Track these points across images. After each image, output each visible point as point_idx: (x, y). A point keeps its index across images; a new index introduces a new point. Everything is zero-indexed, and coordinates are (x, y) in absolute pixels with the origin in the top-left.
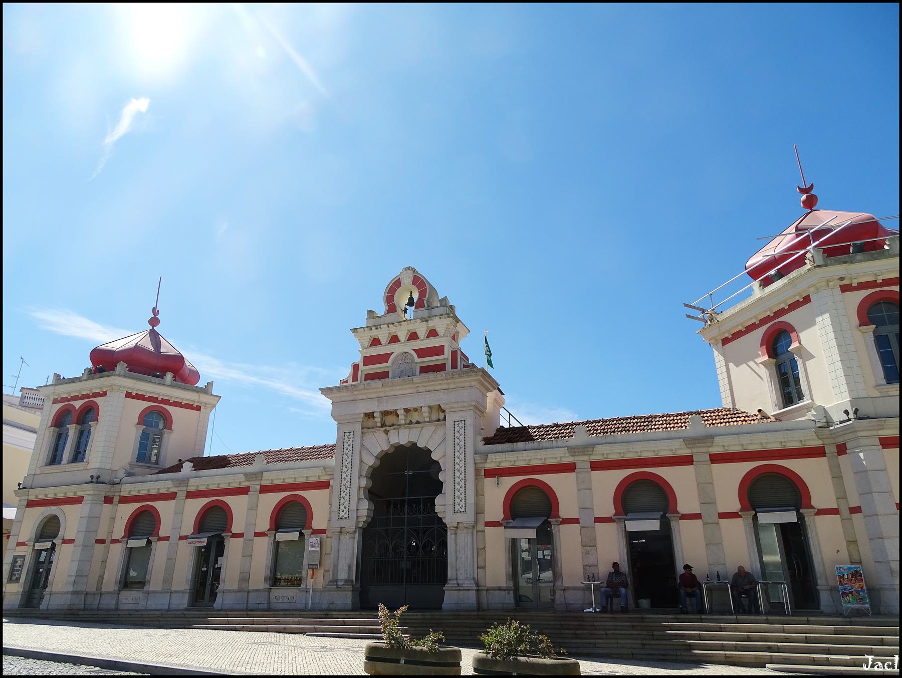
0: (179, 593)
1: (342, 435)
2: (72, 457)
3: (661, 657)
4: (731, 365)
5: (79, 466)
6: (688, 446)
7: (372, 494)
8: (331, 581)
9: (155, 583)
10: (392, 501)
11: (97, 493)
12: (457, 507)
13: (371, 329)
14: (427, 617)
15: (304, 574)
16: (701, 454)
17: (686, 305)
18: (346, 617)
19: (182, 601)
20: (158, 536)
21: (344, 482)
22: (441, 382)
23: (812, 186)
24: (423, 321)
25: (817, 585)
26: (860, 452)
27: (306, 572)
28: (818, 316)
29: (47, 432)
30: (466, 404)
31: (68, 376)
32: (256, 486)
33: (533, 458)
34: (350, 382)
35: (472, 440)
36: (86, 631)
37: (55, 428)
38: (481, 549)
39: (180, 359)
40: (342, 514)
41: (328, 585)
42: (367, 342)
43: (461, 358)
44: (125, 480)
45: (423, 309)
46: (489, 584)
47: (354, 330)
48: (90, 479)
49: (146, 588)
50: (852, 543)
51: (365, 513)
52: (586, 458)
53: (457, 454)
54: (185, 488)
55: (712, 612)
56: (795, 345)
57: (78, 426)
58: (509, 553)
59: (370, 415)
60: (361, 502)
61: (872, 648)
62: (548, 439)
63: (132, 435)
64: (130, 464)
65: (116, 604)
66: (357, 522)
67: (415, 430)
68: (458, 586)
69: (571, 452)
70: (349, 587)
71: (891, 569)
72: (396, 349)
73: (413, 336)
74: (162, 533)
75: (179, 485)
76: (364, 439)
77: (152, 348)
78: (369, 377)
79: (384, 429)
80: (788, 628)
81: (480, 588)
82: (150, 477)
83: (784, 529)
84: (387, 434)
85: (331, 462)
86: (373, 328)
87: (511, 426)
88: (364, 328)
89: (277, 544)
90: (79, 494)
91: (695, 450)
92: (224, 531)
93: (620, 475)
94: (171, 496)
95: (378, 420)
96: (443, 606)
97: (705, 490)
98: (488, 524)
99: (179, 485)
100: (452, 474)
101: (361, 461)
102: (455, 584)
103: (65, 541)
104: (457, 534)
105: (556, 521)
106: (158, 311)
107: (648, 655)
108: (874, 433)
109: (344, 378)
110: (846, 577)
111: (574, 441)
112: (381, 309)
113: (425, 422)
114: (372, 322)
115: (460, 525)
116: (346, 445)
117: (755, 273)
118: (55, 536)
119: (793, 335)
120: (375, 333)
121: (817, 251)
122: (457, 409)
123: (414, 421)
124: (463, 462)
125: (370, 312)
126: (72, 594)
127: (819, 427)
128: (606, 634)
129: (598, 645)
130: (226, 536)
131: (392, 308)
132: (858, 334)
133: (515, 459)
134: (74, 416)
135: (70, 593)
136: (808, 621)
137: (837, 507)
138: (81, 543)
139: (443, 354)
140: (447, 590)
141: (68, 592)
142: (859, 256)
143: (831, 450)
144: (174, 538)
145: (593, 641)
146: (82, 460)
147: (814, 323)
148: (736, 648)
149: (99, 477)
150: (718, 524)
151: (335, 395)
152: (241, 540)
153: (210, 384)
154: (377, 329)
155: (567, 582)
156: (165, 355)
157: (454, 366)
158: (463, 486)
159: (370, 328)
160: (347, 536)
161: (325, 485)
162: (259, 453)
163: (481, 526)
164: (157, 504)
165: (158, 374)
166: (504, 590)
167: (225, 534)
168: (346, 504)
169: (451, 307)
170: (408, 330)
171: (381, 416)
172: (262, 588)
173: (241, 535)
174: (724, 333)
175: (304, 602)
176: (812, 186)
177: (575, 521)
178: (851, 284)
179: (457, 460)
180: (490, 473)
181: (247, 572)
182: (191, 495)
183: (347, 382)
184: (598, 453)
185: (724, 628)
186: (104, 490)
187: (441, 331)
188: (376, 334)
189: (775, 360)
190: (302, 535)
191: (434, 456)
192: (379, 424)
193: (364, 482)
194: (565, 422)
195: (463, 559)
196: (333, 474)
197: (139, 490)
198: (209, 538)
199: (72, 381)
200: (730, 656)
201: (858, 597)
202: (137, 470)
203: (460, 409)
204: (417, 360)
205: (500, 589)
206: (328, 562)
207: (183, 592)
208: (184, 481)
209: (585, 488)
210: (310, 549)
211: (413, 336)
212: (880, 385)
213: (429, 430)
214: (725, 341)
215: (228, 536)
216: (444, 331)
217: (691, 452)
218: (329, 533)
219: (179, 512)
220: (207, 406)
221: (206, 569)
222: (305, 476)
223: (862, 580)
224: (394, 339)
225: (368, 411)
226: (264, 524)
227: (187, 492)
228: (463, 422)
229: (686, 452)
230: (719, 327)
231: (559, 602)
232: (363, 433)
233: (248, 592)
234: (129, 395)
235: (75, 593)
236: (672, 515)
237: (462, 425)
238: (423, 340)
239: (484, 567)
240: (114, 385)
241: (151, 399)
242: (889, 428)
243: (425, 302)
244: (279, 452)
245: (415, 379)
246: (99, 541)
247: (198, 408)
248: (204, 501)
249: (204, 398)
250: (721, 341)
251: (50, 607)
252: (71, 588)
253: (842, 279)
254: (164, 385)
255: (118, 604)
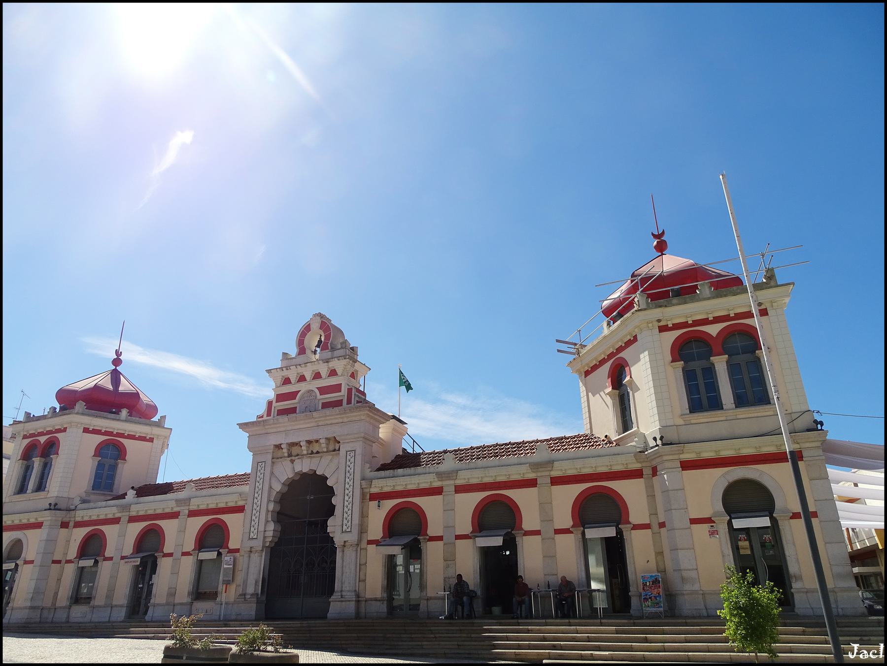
0: (185, 605)
1: (256, 464)
2: (18, 489)
3: (467, 656)
4: (590, 394)
5: (41, 494)
6: (533, 470)
7: (280, 517)
8: (240, 595)
9: (99, 599)
10: (319, 521)
11: (54, 518)
12: (345, 527)
13: (283, 370)
14: (304, 625)
15: (220, 589)
16: (543, 478)
17: (558, 341)
18: (240, 626)
19: (120, 614)
20: (104, 556)
21: (255, 506)
22: (336, 417)
23: (663, 232)
24: (325, 363)
25: (630, 591)
26: (665, 474)
27: (221, 587)
28: (641, 353)
29: (17, 464)
30: (356, 436)
31: (38, 414)
32: (185, 511)
33: (408, 483)
34: (265, 418)
35: (358, 467)
36: (110, 642)
37: (41, 458)
38: (363, 565)
39: (136, 396)
40: (252, 535)
41: (237, 598)
42: (279, 381)
43: (355, 394)
44: (80, 506)
45: (327, 351)
46: (369, 595)
47: (269, 371)
48: (48, 507)
49: (92, 603)
50: (660, 554)
51: (271, 534)
52: (452, 482)
53: (347, 480)
54: (128, 514)
55: (537, 618)
56: (628, 378)
57: (24, 461)
58: (385, 567)
59: (278, 447)
60: (268, 524)
61: (632, 645)
62: (564, 450)
63: (87, 466)
64: (85, 492)
65: (66, 618)
66: (264, 542)
67: (315, 459)
68: (342, 598)
69: (439, 477)
70: (254, 599)
71: (682, 577)
72: (303, 387)
73: (317, 376)
74: (107, 554)
75: (122, 511)
76: (274, 467)
77: (111, 387)
78: (281, 412)
79: (290, 459)
80: (580, 629)
81: (360, 599)
82: (100, 504)
83: (607, 541)
84: (293, 463)
85: (245, 489)
86: (284, 369)
87: (415, 452)
88: (276, 369)
89: (201, 563)
90: (40, 520)
91: (539, 474)
92: (157, 551)
93: (577, 489)
94: (115, 521)
95: (285, 451)
96: (329, 615)
97: (545, 507)
98: (370, 542)
99: (122, 511)
100: (342, 498)
101: (271, 487)
102: (339, 596)
103: (26, 562)
104: (345, 552)
105: (425, 539)
106: (121, 352)
107: (457, 654)
108: (676, 457)
109: (260, 413)
110: (648, 584)
111: (442, 468)
112: (293, 351)
113: (324, 452)
114: (286, 363)
115: (347, 544)
116: (259, 474)
117: (607, 312)
118: (18, 558)
119: (627, 369)
120: (286, 373)
121: (642, 296)
122: (349, 441)
123: (315, 451)
124: (352, 487)
125: (285, 354)
126: (29, 609)
127: (640, 452)
128: (435, 637)
129: (424, 647)
130: (158, 555)
131: (302, 351)
132: (670, 370)
133: (395, 484)
134: (38, 451)
135: (28, 608)
136: (601, 623)
137: (649, 523)
138: (39, 564)
139: (341, 392)
140: (332, 601)
141: (26, 608)
142: (675, 301)
143: (647, 472)
144: (177, 555)
145: (420, 643)
146: (44, 490)
147: (639, 360)
148: (529, 647)
149: (56, 504)
150: (553, 539)
151: (250, 429)
152: (440, 543)
153: (163, 418)
154: (287, 369)
155: (430, 593)
156: (123, 393)
157: (349, 402)
158: (351, 508)
159: (281, 369)
160: (256, 554)
161: (240, 509)
162: (191, 481)
163: (364, 544)
164: (162, 523)
165: (114, 410)
166: (379, 600)
167: (158, 554)
168: (256, 526)
169: (352, 349)
170: (313, 371)
171: (288, 448)
172: (64, 605)
173: (170, 555)
174: (585, 366)
175: (219, 614)
176: (663, 232)
177: (440, 538)
178: (729, 315)
179: (347, 486)
180: (374, 497)
181: (173, 588)
182: (133, 519)
183: (262, 417)
184: (461, 477)
185: (531, 630)
186: (60, 516)
187: (339, 372)
188: (286, 374)
189: (618, 391)
190: (219, 554)
191: (329, 483)
192: (286, 455)
193: (271, 507)
194: (530, 439)
195: (348, 573)
196: (247, 500)
197: (172, 508)
198: (142, 558)
199: (39, 418)
200: (518, 653)
201: (655, 601)
202: (92, 497)
203: (352, 440)
204: (319, 396)
205: (376, 600)
206: (240, 578)
207: (121, 606)
208: (127, 507)
209: (449, 509)
210: (225, 566)
211: (317, 376)
212: (684, 415)
213: (327, 458)
214: (587, 373)
215: (160, 555)
216: (341, 371)
217: (535, 475)
218: (242, 552)
219: (122, 535)
220: (159, 437)
221: (142, 586)
222: (225, 501)
223: (659, 587)
224: (302, 379)
225: (278, 443)
226: (190, 545)
227: (130, 517)
228: (354, 452)
229: (531, 476)
230: (581, 361)
231: (423, 611)
232: (273, 463)
233: (174, 605)
234: (86, 430)
235: (32, 608)
236: (517, 532)
237: (352, 454)
238: (325, 379)
239: (364, 581)
240: (73, 422)
241: (107, 433)
242: (687, 453)
243: (329, 344)
244: (244, 476)
245: (315, 414)
246: (54, 562)
247: (151, 440)
248: (205, 519)
249: (156, 431)
250: (583, 373)
251: (11, 621)
252: (29, 604)
253: (659, 321)
254: (118, 420)
255: (69, 617)
